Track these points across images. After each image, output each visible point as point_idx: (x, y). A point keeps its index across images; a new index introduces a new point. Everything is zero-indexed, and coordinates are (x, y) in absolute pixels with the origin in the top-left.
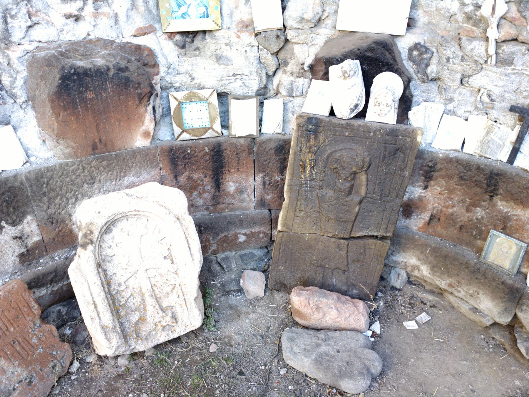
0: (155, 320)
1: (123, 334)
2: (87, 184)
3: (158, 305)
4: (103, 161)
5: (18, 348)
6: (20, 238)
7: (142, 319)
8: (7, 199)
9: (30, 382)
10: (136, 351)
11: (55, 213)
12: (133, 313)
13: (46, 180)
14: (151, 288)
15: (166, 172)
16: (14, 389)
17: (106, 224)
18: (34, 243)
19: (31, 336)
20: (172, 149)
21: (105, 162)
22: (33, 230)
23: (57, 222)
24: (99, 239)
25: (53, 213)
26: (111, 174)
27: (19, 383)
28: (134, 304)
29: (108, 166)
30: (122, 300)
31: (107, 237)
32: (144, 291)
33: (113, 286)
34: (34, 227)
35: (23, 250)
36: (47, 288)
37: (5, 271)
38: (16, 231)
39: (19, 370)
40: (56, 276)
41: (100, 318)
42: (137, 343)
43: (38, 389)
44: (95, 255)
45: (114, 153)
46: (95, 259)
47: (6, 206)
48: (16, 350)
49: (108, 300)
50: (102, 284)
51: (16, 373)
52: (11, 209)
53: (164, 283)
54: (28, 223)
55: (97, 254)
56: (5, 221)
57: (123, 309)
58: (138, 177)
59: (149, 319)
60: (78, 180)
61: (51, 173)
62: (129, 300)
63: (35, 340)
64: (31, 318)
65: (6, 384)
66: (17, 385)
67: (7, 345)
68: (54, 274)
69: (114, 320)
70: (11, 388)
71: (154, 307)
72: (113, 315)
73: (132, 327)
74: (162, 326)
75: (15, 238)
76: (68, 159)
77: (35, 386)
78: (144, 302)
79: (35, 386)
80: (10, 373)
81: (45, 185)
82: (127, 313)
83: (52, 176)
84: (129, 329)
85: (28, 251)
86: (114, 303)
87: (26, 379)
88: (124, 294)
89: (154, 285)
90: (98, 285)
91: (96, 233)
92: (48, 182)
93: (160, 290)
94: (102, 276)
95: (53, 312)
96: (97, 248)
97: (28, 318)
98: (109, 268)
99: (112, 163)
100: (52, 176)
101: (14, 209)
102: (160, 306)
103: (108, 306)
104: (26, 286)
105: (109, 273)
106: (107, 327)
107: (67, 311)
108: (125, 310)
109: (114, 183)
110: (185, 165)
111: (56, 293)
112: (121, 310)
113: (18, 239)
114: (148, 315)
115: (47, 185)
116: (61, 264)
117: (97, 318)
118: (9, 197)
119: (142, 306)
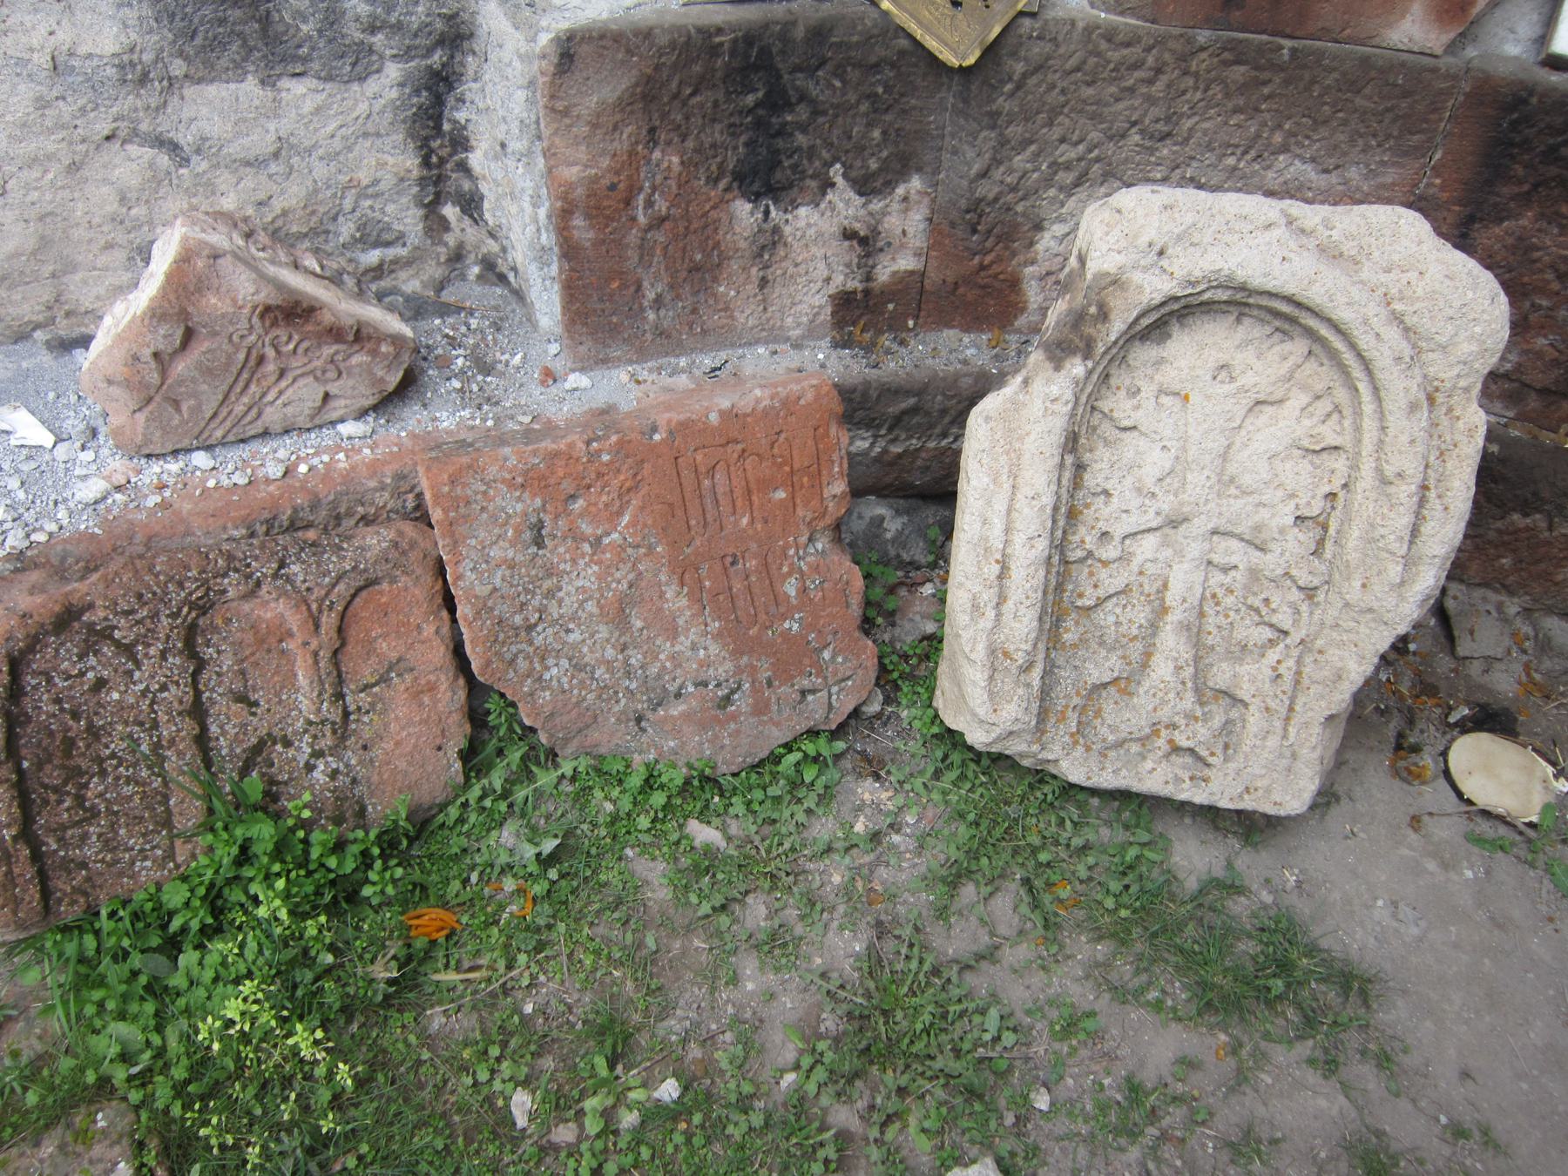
0: (1159, 713)
1: (1042, 700)
2: (1142, 132)
3: (1191, 670)
4: (1237, 62)
5: (737, 586)
6: (864, 241)
7: (1123, 685)
8: (880, 90)
9: (727, 700)
10: (1054, 771)
11: (996, 199)
12: (1104, 653)
13: (1020, 68)
14: (1196, 603)
15: (1442, 188)
16: (678, 695)
17: (1163, 304)
18: (895, 273)
19: (785, 569)
20: (1525, 102)
21: (1242, 69)
22: (911, 231)
23: (989, 232)
24: (1114, 351)
25: (991, 196)
26: (1239, 126)
27: (696, 685)
28: (1118, 624)
29: (1244, 88)
30: (1089, 591)
31: (1144, 354)
32: (1171, 598)
33: (1082, 530)
34: (916, 223)
35: (854, 284)
36: (876, 437)
37: (781, 327)
38: (862, 212)
39: (714, 649)
40: (914, 410)
41: (999, 615)
42: (1068, 750)
43: (738, 732)
44: (1077, 399)
45: (1288, 43)
46: (1073, 415)
47: (866, 115)
48: (730, 589)
49: (1048, 572)
50: (1056, 509)
51: (702, 652)
52: (876, 134)
53: (1250, 607)
54: (905, 199)
55: (1083, 399)
56: (844, 165)
57: (1077, 623)
58: (1326, 171)
59: (1143, 699)
60: (1121, 106)
61: (1048, 47)
62: (1109, 605)
63: (791, 588)
64: (809, 516)
65: (664, 667)
66: (691, 689)
67: (712, 558)
68: (912, 401)
69: (1035, 645)
70: (672, 688)
71: (1178, 668)
72: (1041, 630)
73: (1078, 693)
74: (1171, 741)
75: (848, 235)
76: (1122, 13)
77: (733, 717)
78: (1154, 635)
79: (733, 717)
80: (688, 643)
81: (1008, 87)
82: (1083, 641)
83: (1048, 58)
84: (1067, 690)
85: (867, 292)
86: (1060, 588)
87: (718, 685)
88: (1103, 574)
89: (1214, 596)
90: (1042, 508)
91: (1117, 326)
92: (1025, 76)
93: (1221, 620)
94: (1065, 482)
95: (860, 517)
96: (1095, 377)
97: (800, 512)
98: (1097, 466)
99: (1265, 83)
100: (1048, 58)
101: (884, 133)
102: (1196, 676)
103: (1040, 594)
104: (839, 408)
105: (1091, 480)
106: (1006, 654)
107: (900, 533)
108: (1081, 629)
109: (1231, 161)
110: (1536, 186)
111: (891, 464)
112: (1069, 623)
113: (855, 243)
114: (1146, 684)
115: (1018, 87)
116: (944, 379)
117: (991, 614)
118: (888, 89)
119: (1139, 645)
